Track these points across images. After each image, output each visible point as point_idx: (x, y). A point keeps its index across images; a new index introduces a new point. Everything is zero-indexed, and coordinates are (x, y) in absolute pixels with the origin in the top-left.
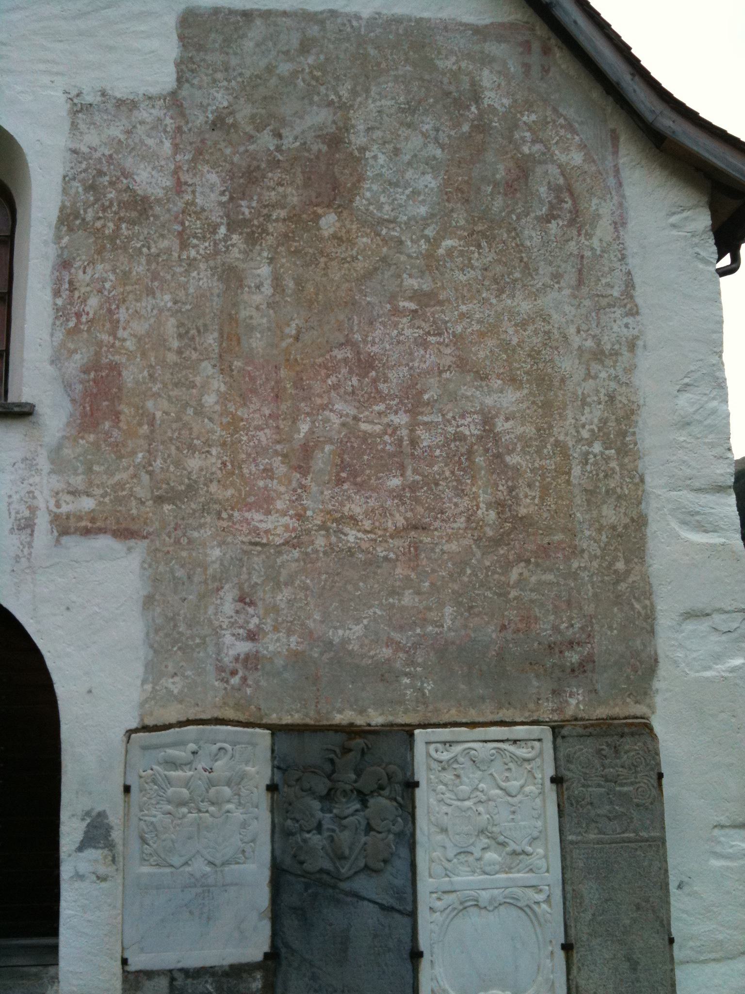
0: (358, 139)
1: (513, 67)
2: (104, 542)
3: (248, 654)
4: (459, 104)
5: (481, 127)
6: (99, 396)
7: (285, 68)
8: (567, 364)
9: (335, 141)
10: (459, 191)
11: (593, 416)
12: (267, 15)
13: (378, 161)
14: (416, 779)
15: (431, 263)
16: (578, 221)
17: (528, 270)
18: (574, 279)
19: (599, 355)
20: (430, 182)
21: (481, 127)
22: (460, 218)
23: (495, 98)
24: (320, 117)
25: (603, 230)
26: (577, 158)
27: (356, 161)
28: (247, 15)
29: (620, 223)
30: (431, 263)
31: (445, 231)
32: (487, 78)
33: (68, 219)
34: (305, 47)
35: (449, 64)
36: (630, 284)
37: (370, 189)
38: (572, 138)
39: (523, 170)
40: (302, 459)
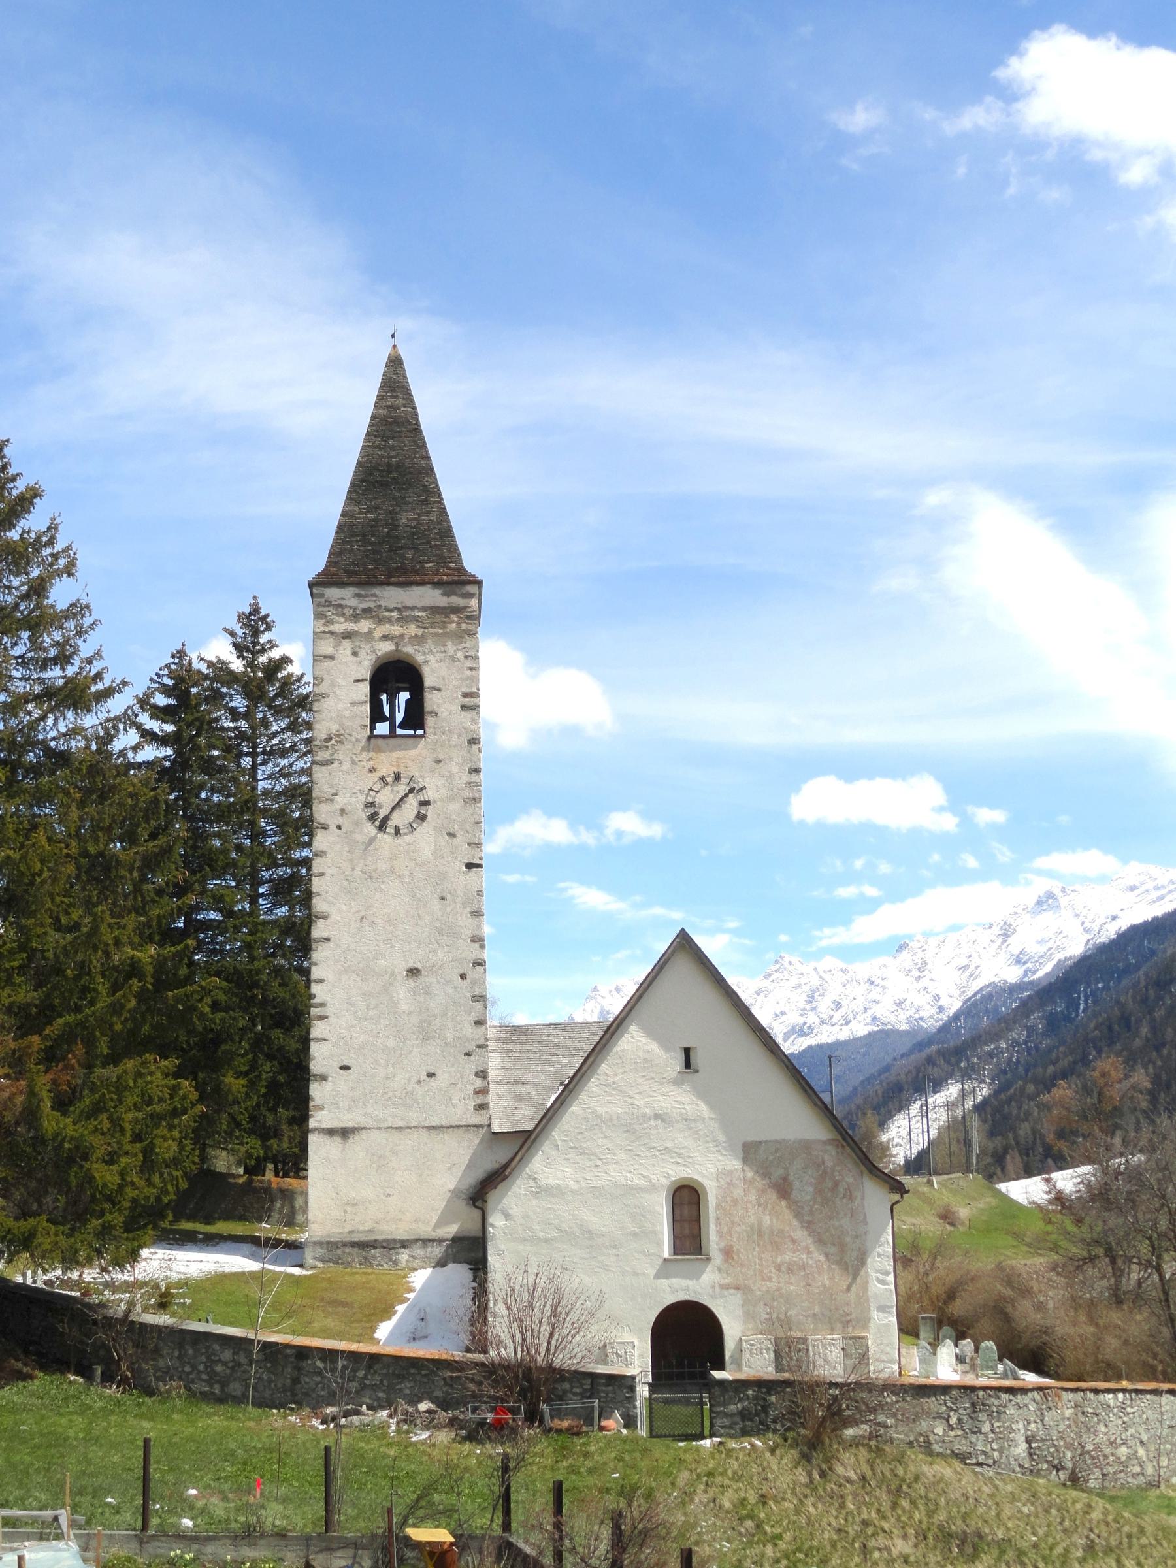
0: (791, 1178)
1: (834, 1153)
2: (732, 1291)
3: (135, 1260)
4: (819, 1165)
5: (825, 1172)
6: (728, 1253)
7: (771, 1158)
8: (848, 1239)
9: (785, 1179)
10: (819, 1191)
11: (854, 1254)
12: (766, 1142)
13: (797, 1184)
14: (686, 1088)
15: (811, 1213)
16: (851, 1198)
17: (838, 1213)
18: (896, 1124)
19: (857, 1237)
20: (811, 1189)
21: (825, 1172)
22: (819, 1199)
23: (829, 1164)
24: (780, 1172)
25: (858, 1201)
26: (851, 1180)
27: (790, 1184)
28: (760, 1142)
29: (863, 1199)
30: (811, 1213)
31: (815, 1203)
32: (826, 1157)
33: (718, 1207)
34: (776, 1151)
35: (816, 1153)
36: (865, 1216)
37: (795, 1193)
38: (849, 1174)
39: (836, 1184)
40: (778, 1268)
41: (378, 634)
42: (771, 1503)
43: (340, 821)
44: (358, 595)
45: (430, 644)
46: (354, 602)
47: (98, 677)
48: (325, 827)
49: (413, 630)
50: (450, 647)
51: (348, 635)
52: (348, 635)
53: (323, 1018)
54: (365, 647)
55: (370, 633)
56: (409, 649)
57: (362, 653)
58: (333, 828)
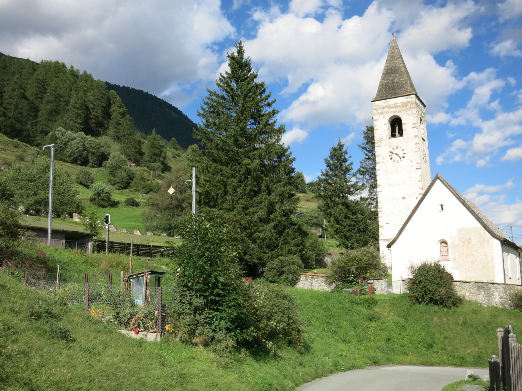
6: (455, 259)
33: (451, 246)
39: (484, 239)
41: (389, 112)
42: (284, 269)
43: (383, 161)
44: (384, 102)
45: (403, 112)
46: (383, 104)
47: (203, 109)
48: (379, 163)
49: (398, 109)
50: (408, 112)
51: (382, 113)
52: (382, 113)
53: (381, 211)
54: (387, 115)
55: (388, 111)
56: (398, 114)
57: (386, 117)
58: (381, 162)
